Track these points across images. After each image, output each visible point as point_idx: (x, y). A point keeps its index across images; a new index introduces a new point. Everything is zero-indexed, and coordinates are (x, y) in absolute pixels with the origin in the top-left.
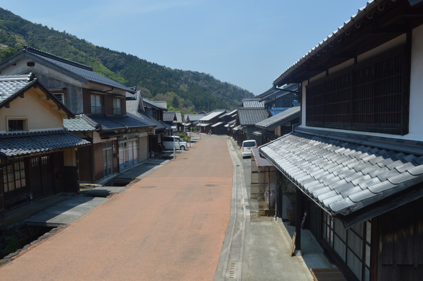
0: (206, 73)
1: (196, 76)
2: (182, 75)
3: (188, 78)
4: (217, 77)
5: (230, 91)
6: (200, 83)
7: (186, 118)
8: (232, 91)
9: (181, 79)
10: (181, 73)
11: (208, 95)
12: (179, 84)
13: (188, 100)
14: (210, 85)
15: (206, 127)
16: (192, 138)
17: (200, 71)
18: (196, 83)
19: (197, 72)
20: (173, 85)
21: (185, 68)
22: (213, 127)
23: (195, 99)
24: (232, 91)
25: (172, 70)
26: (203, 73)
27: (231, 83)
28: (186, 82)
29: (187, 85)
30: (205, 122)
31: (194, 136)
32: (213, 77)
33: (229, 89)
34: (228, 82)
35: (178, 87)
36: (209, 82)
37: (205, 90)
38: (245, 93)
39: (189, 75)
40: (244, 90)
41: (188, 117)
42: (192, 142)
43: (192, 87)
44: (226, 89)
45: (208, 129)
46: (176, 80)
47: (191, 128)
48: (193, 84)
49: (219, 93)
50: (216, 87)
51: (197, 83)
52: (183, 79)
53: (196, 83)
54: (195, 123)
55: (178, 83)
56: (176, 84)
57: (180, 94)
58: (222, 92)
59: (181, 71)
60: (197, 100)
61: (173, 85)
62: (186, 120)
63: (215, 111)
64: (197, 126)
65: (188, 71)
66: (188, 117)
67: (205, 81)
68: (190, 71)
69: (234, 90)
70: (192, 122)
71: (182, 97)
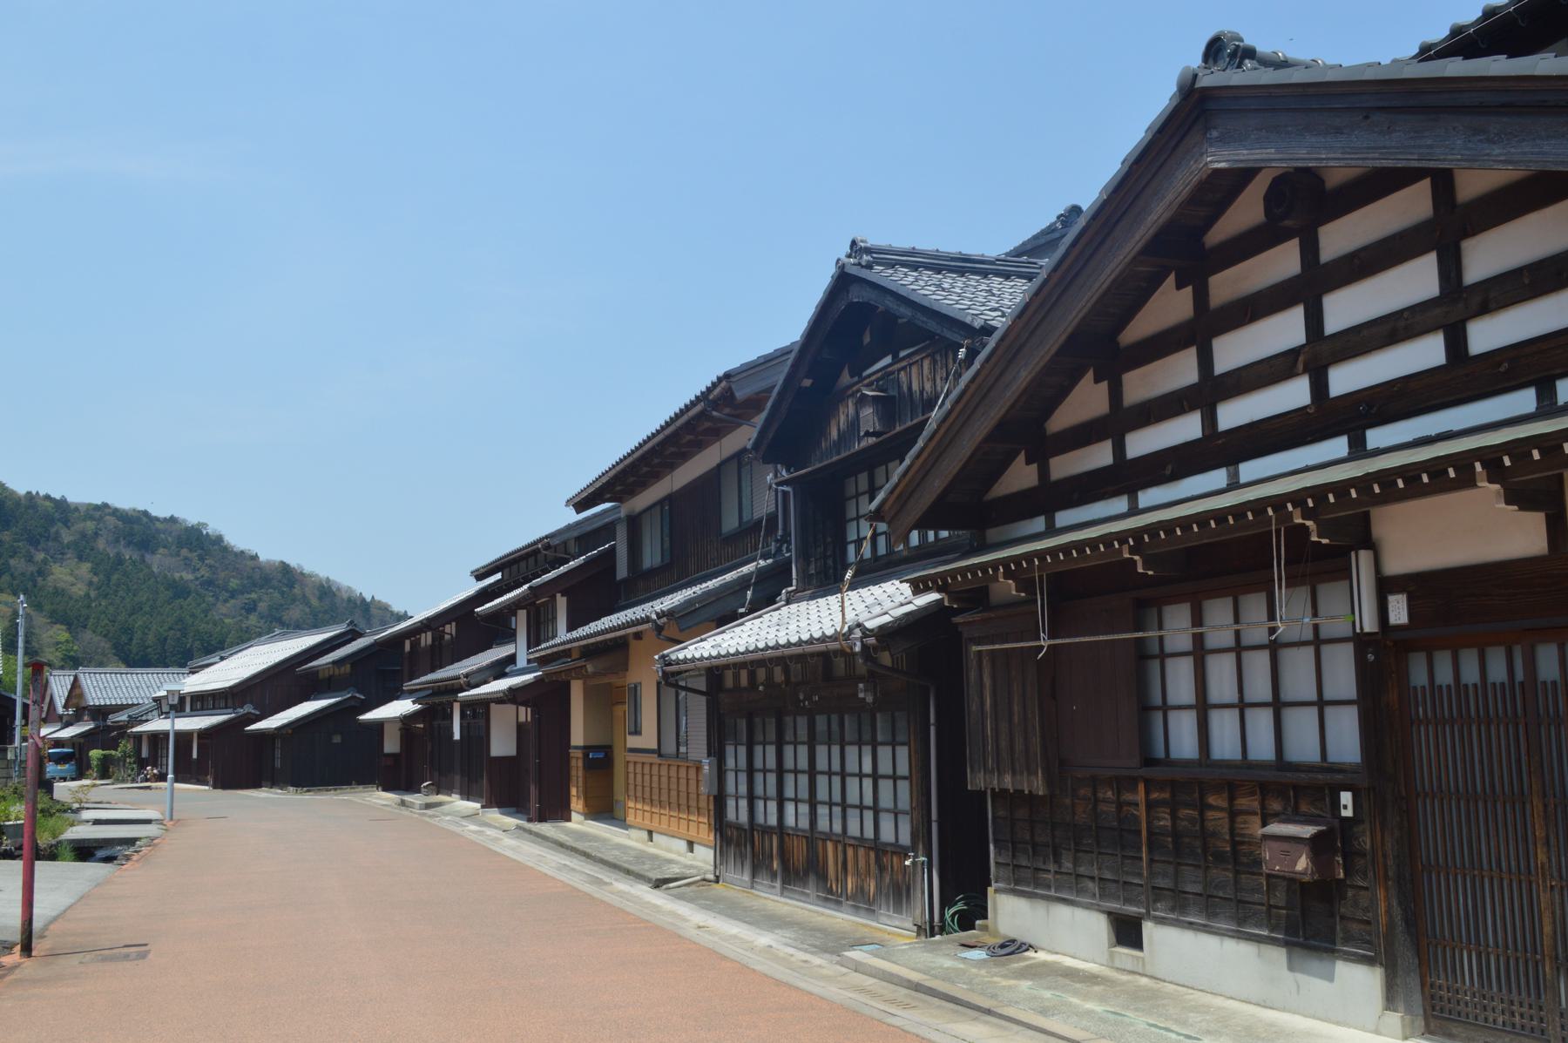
0: (191, 517)
1: (139, 531)
2: (66, 523)
3: (96, 534)
4: (238, 539)
5: (305, 600)
6: (158, 561)
7: (59, 685)
8: (315, 602)
9: (57, 538)
10: (62, 510)
11: (193, 615)
12: (45, 562)
13: (88, 635)
14: (204, 572)
15: (204, 734)
16: (86, 815)
17: (160, 511)
18: (136, 557)
19: (145, 513)
20: (12, 562)
21: (80, 491)
22: (262, 734)
23: (128, 630)
24: (315, 602)
25: (13, 493)
26: (173, 520)
27: (307, 569)
28: (83, 549)
29: (85, 567)
30: (202, 702)
31: (100, 805)
32: (220, 539)
33: (297, 590)
34: (293, 563)
35: (41, 573)
36: (201, 559)
37: (180, 591)
38: (374, 611)
39: (100, 519)
40: (369, 599)
41: (76, 684)
42: (85, 851)
43: (115, 577)
44: (282, 593)
45: (233, 755)
46: (34, 541)
47: (95, 754)
48: (119, 561)
49: (251, 608)
50: (234, 583)
51: (143, 561)
52: (67, 537)
53: (136, 557)
54: (123, 717)
55: (40, 556)
56: (30, 559)
57: (47, 607)
58: (262, 606)
59: (61, 505)
60: (138, 635)
61: (12, 562)
62: (60, 703)
63: (273, 640)
64: (138, 737)
65: (97, 508)
66: (76, 684)
67: (185, 552)
68: (106, 505)
69: (320, 599)
70: (100, 712)
71: (57, 618)
